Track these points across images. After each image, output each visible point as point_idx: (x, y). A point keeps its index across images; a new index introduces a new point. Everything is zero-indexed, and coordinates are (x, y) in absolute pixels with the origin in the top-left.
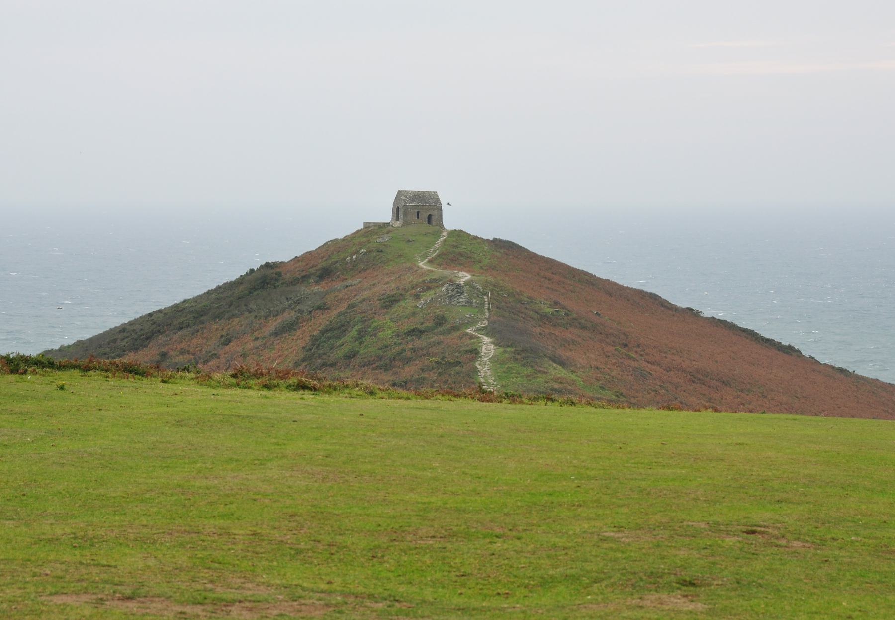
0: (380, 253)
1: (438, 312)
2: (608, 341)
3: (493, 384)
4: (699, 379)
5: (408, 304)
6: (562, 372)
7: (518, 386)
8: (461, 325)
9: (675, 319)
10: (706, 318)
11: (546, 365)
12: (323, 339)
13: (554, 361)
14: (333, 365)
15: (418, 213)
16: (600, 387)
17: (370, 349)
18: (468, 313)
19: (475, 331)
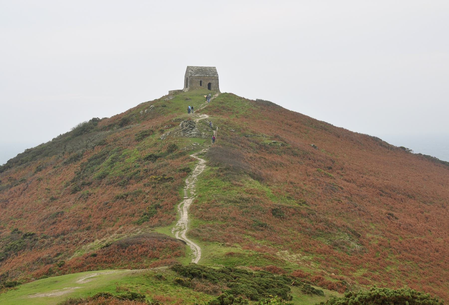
0: (164, 108)
1: (173, 142)
2: (314, 164)
3: (193, 195)
4: (386, 193)
5: (153, 138)
6: (257, 185)
7: (213, 196)
8: (187, 151)
9: (389, 154)
10: (416, 154)
11: (243, 180)
12: (89, 165)
13: (253, 177)
14: (89, 184)
15: (201, 82)
16: (287, 197)
17: (116, 171)
18: (194, 142)
19: (196, 156)
